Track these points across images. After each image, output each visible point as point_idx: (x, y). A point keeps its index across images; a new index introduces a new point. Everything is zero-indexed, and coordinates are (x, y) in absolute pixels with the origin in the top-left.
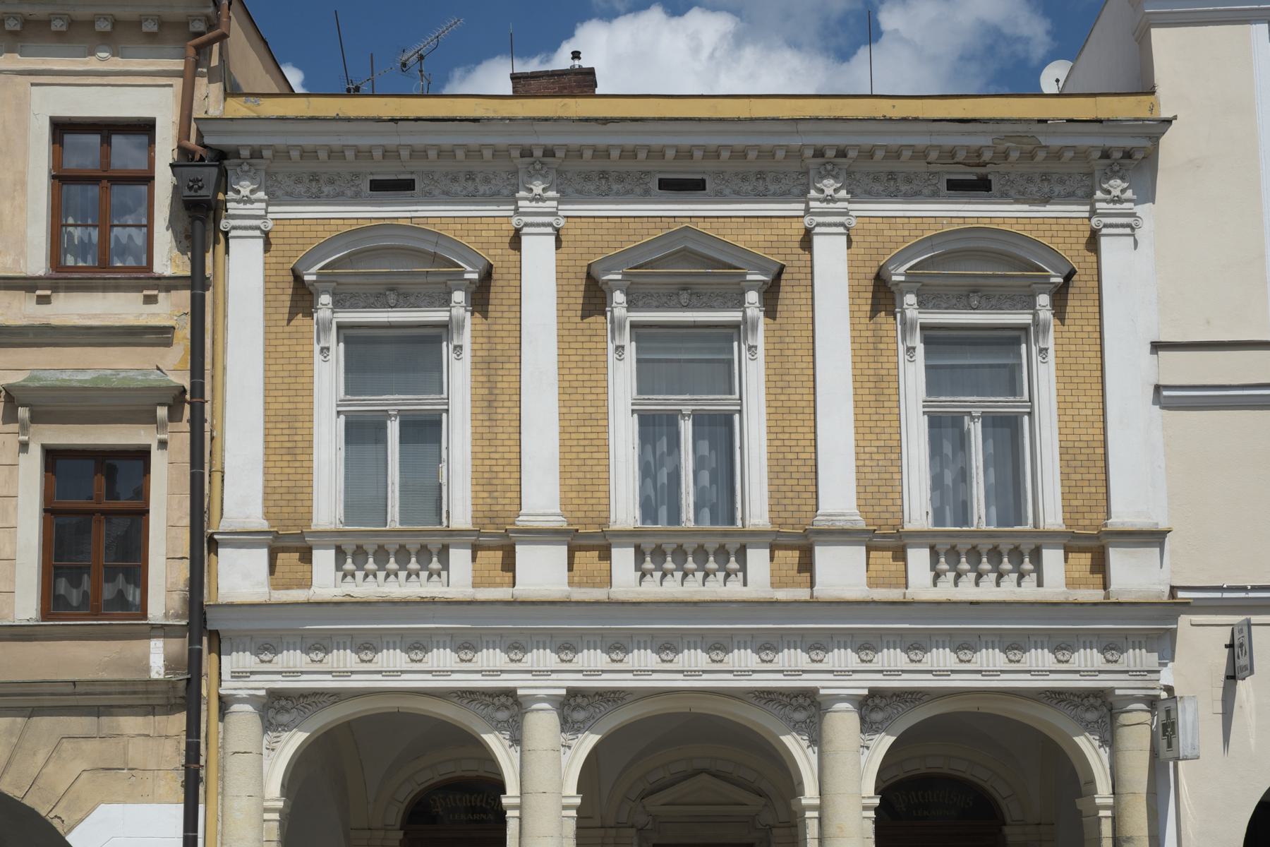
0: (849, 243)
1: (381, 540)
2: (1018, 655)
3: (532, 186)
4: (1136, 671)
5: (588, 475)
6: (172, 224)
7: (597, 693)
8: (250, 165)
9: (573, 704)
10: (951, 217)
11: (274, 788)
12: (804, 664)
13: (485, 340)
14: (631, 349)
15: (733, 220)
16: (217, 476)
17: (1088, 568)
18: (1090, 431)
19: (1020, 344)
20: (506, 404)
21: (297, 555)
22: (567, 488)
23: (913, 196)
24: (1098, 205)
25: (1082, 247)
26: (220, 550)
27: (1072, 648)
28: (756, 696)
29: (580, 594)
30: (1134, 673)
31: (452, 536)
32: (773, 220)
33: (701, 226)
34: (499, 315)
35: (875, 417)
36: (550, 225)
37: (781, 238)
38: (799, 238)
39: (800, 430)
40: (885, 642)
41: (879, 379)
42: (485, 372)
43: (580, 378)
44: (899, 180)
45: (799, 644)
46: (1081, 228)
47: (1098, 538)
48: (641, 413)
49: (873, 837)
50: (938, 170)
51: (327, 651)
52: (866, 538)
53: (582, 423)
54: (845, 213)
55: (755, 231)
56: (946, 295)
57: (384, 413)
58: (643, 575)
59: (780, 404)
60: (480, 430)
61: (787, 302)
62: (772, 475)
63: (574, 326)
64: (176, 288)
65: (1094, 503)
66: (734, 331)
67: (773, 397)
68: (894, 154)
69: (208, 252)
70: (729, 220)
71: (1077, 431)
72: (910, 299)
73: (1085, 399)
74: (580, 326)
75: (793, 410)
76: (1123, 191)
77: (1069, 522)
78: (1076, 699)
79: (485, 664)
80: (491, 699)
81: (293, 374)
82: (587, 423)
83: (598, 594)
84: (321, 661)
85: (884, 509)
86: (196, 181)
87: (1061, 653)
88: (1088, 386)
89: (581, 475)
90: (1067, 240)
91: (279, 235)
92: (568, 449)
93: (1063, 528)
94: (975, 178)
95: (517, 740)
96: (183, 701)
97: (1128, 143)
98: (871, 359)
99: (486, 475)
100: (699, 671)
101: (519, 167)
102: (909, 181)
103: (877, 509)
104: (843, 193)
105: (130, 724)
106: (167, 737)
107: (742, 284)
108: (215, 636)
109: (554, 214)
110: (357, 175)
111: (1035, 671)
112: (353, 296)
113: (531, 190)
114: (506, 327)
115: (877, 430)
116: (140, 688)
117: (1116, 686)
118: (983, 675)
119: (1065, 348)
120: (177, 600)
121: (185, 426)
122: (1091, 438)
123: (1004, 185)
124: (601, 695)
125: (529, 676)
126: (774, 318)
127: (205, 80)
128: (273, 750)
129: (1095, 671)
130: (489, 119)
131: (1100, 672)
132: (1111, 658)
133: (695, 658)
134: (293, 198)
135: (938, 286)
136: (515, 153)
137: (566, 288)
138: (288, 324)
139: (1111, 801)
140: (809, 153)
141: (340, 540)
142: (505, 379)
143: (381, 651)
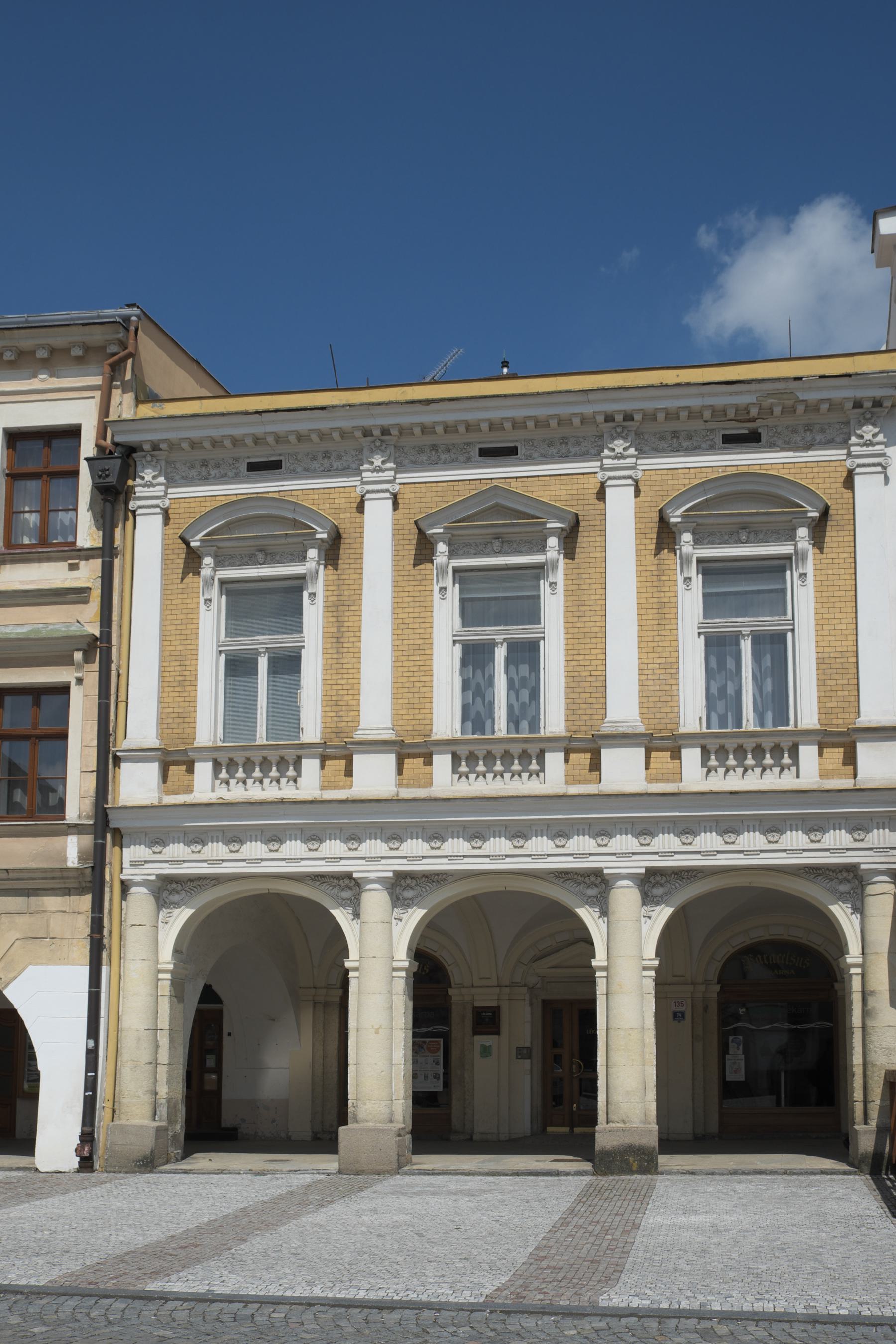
0: (637, 493)
1: (248, 753)
2: (776, 836)
3: (373, 460)
4: (880, 848)
5: (416, 696)
6: (91, 507)
7: (673, 872)
8: (152, 456)
9: (404, 884)
10: (726, 466)
11: (166, 955)
12: (848, 844)
13: (336, 588)
14: (698, 581)
15: (540, 478)
16: (122, 706)
17: (841, 760)
18: (844, 643)
19: (785, 571)
20: (351, 639)
21: (184, 767)
22: (398, 707)
23: (694, 450)
24: (853, 449)
25: (840, 485)
26: (122, 764)
27: (823, 830)
28: (807, 872)
29: (406, 793)
30: (878, 850)
31: (303, 748)
32: (574, 477)
33: (515, 487)
34: (347, 567)
35: (657, 638)
36: (630, 477)
37: (580, 492)
38: (596, 491)
39: (593, 651)
40: (832, 824)
41: (661, 606)
42: (334, 614)
43: (411, 615)
44: (681, 437)
45: (587, 831)
46: (839, 469)
47: (849, 734)
48: (707, 635)
49: (653, 992)
50: (714, 427)
51: (204, 843)
52: (645, 740)
53: (411, 652)
54: (633, 468)
55: (559, 487)
56: (719, 532)
57: (254, 651)
58: (709, 771)
59: (576, 630)
60: (329, 661)
61: (584, 545)
62: (569, 691)
63: (407, 573)
64: (93, 557)
65: (847, 704)
66: (539, 570)
67: (571, 625)
68: (671, 415)
69: (118, 527)
70: (537, 479)
71: (833, 644)
72: (687, 537)
73: (840, 616)
74: (412, 573)
75: (588, 635)
76: (874, 435)
77: (824, 722)
78: (831, 873)
79: (328, 852)
80: (835, 874)
81: (184, 622)
82: (416, 652)
83: (421, 793)
84: (199, 852)
85: (664, 715)
86: (103, 471)
87: (857, 833)
88: (843, 605)
89: (410, 695)
90: (827, 480)
91: (177, 511)
92: (400, 674)
93: (818, 727)
94: (747, 432)
95: (604, 913)
96: (88, 885)
97: (878, 393)
98: (655, 590)
99: (334, 698)
100: (502, 856)
101: (364, 444)
102: (690, 437)
103: (658, 716)
104: (632, 451)
105: (52, 903)
106: (79, 913)
107: (544, 531)
108: (117, 833)
109: (633, 468)
110: (237, 460)
111: (790, 850)
112: (232, 556)
113: (373, 463)
114: (352, 577)
115: (660, 649)
116: (58, 874)
117: (861, 861)
118: (745, 855)
119: (823, 572)
120: (88, 805)
121: (96, 666)
122: (845, 649)
123: (772, 437)
124: (677, 874)
125: (363, 862)
126: (573, 559)
127: (119, 391)
128: (166, 923)
129: (843, 849)
130: (333, 407)
131: (848, 849)
132: (857, 837)
133: (499, 845)
134: (188, 481)
135: (713, 524)
136: (358, 434)
137: (401, 542)
138: (181, 582)
139: (860, 960)
140: (600, 419)
141: (215, 754)
142: (351, 619)
143: (246, 843)
